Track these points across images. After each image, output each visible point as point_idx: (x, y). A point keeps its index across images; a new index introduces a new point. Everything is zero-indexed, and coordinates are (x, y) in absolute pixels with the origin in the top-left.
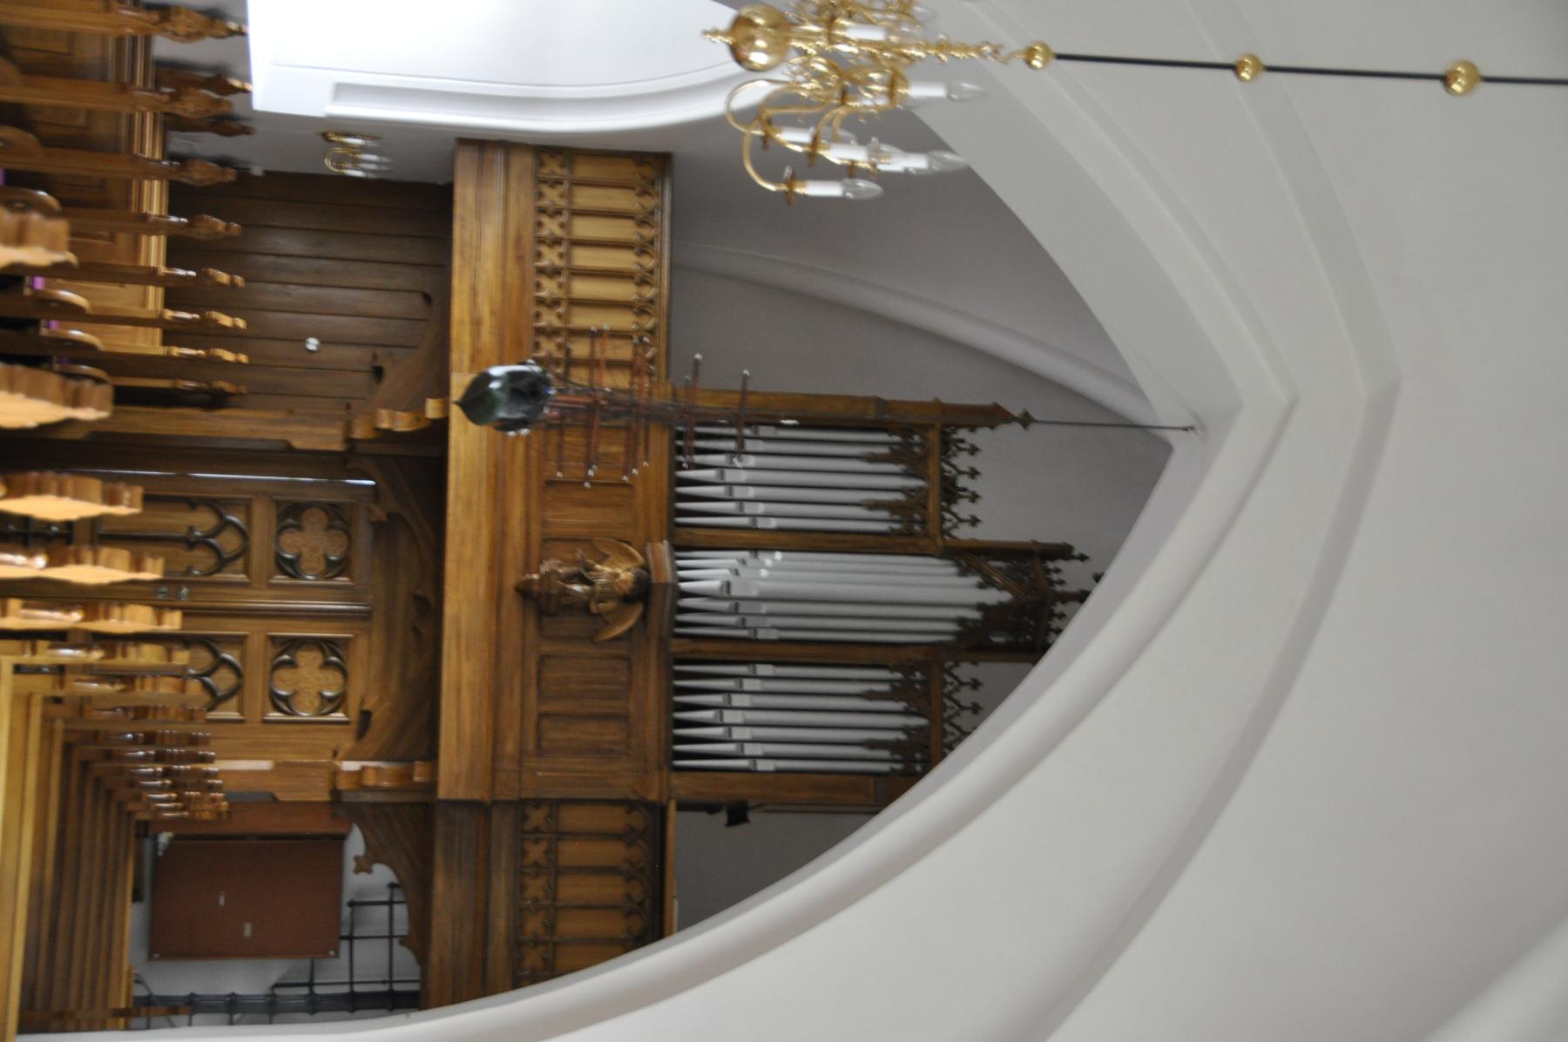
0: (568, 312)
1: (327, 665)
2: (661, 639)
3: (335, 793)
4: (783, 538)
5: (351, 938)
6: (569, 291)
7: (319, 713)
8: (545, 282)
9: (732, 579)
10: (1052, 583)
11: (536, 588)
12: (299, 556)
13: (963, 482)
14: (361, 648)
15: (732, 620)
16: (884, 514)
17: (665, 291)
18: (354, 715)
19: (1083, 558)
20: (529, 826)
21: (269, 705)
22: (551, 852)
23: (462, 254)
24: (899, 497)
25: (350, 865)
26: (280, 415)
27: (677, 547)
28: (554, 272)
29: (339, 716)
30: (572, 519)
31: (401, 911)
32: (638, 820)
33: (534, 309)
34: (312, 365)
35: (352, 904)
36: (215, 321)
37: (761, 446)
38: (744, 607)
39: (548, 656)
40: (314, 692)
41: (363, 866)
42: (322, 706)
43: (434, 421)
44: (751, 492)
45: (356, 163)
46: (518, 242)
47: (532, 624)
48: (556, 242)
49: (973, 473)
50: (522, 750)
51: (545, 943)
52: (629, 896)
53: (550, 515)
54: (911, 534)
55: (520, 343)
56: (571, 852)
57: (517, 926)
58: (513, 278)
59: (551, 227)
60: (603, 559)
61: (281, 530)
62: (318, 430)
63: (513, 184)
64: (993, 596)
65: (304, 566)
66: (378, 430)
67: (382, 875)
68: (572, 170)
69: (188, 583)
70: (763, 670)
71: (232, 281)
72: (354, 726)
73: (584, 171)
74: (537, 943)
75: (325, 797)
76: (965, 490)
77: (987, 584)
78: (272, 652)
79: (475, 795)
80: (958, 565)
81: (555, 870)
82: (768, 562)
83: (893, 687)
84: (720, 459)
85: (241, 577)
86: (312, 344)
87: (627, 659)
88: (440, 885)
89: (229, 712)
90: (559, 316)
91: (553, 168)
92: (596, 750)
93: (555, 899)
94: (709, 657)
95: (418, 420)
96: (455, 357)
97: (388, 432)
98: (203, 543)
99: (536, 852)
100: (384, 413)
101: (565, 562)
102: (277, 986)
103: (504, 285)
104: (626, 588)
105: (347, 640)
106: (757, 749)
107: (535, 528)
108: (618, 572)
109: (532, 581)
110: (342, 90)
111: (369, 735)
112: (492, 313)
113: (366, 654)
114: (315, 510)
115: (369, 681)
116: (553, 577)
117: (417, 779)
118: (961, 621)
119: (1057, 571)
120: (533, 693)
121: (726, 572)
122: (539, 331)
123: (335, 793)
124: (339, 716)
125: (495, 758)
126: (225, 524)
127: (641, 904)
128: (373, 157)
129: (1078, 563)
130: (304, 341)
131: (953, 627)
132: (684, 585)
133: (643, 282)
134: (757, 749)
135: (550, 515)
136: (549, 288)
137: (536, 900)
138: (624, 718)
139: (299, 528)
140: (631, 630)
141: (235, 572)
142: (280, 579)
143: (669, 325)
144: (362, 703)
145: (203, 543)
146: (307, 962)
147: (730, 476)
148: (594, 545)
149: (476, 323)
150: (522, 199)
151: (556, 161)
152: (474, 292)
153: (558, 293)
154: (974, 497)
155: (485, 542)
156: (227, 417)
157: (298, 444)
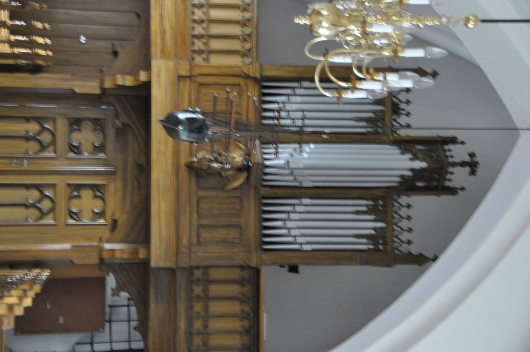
1: (96, 196)
5: (110, 322)
7: (93, 219)
8: (196, 11)
9: (290, 159)
10: (447, 157)
11: (196, 165)
13: (402, 106)
14: (112, 187)
16: (364, 240)
17: (255, 15)
18: (109, 221)
19: (462, 143)
20: (194, 278)
21: (68, 216)
22: (205, 290)
24: (371, 115)
25: (109, 292)
26: (69, 76)
28: (200, 52)
29: (102, 221)
31: (133, 309)
32: (246, 274)
33: (191, 25)
34: (84, 50)
35: (110, 307)
37: (303, 91)
38: (296, 172)
39: (202, 198)
41: (116, 292)
47: (194, 180)
49: (408, 102)
50: (190, 244)
51: (203, 334)
52: (243, 311)
54: (377, 133)
55: (184, 43)
56: (215, 290)
57: (190, 326)
61: (71, 131)
64: (419, 164)
65: (83, 148)
67: (124, 295)
69: (27, 158)
72: (109, 226)
74: (199, 333)
75: (96, 261)
76: (403, 110)
77: (415, 158)
78: (68, 190)
79: (169, 265)
80: (401, 148)
81: (206, 298)
82: (307, 150)
83: (369, 209)
85: (53, 155)
86: (83, 39)
87: (240, 198)
88: (153, 306)
89: (49, 220)
90: (204, 28)
92: (225, 242)
95: (136, 80)
98: (33, 138)
99: (198, 290)
102: (78, 344)
103: (177, 14)
104: (239, 164)
105: (104, 185)
109: (192, 162)
112: (171, 28)
113: (114, 190)
118: (402, 177)
119: (450, 150)
120: (195, 216)
122: (195, 36)
123: (102, 260)
124: (102, 221)
125: (178, 246)
126: (44, 129)
127: (249, 315)
129: (460, 146)
130: (78, 38)
131: (398, 179)
133: (245, 10)
137: (198, 313)
138: (238, 226)
139: (80, 130)
141: (49, 152)
142: (72, 155)
143: (257, 33)
144: (113, 215)
146: (90, 334)
149: (163, 33)
152: (162, 17)
153: (203, 17)
154: (408, 114)
157: (78, 90)
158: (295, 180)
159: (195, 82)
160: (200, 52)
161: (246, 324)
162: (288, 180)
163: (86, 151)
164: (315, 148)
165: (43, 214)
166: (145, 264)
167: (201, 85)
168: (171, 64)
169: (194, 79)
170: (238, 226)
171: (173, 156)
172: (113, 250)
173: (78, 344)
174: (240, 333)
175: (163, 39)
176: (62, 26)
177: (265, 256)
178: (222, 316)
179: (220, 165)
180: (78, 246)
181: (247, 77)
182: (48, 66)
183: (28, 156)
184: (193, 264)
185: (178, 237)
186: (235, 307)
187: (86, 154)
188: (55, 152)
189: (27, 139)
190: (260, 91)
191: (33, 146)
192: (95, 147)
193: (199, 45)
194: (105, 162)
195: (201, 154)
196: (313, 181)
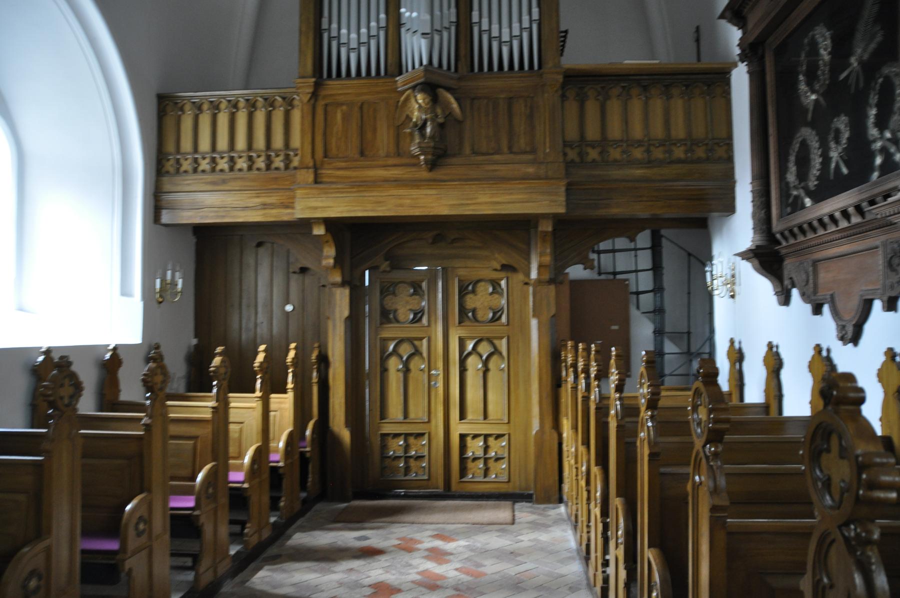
0: (256, 151)
1: (474, 291)
2: (459, 79)
3: (551, 281)
4: (391, 9)
6: (243, 152)
8: (238, 166)
12: (411, 310)
14: (462, 272)
15: (445, 34)
18: (502, 274)
20: (577, 160)
23: (223, 217)
27: (400, 73)
28: (287, 160)
30: (384, 138)
31: (603, 246)
34: (302, 307)
36: (261, 363)
39: (473, 149)
40: (490, 298)
42: (497, 293)
43: (327, 230)
44: (364, 30)
45: (174, 284)
46: (213, 183)
47: (454, 160)
48: (213, 160)
50: (533, 162)
53: (382, 153)
56: (592, 132)
58: (236, 185)
59: (205, 165)
60: (409, 118)
62: (338, 302)
63: (179, 188)
65: (416, 307)
66: (335, 266)
68: (170, 154)
69: (429, 371)
70: (475, 17)
71: (220, 354)
72: (509, 274)
73: (170, 147)
74: (648, 151)
75: (552, 287)
78: (467, 323)
81: (604, 143)
84: (343, 51)
85: (425, 342)
86: (289, 308)
87: (473, 99)
89: (503, 345)
91: (170, 166)
92: (531, 117)
93: (622, 141)
94: (469, 49)
96: (285, 218)
97: (336, 259)
98: (406, 364)
99: (593, 154)
100: (324, 262)
101: (412, 139)
105: (460, 281)
106: (526, 18)
107: (391, 161)
108: (418, 106)
109: (426, 161)
110: (125, 292)
111: (516, 266)
113: (466, 270)
114: (385, 303)
115: (483, 266)
116: (423, 145)
117: (550, 229)
120: (497, 157)
121: (415, 38)
122: (268, 167)
123: (551, 281)
124: (503, 283)
126: (395, 352)
127: (623, 87)
128: (169, 273)
130: (288, 313)
132: (425, 62)
133: (235, 106)
134: (526, 18)
135: (382, 153)
136: (242, 164)
137: (624, 152)
138: (510, 101)
139: (396, 311)
140: (457, 99)
141: (422, 345)
142: (425, 320)
144: (496, 270)
145: (486, 363)
147: (354, 45)
148: (400, 126)
149: (265, 206)
150: (189, 182)
151: (163, 165)
155: (401, 192)
156: (333, 350)
157: (346, 313)
158: (448, 29)
159: (322, 163)
160: (287, 160)
161: (635, 91)
162: (448, 38)
163: (420, 303)
164: (405, 7)
165: (496, 351)
166: (559, 221)
167: (326, 156)
168: (299, 193)
169: (318, 163)
170: (510, 101)
171: (418, 187)
172: (540, 267)
173: (638, 308)
174: (647, 98)
175: (272, 206)
176: (275, 330)
177: (549, 65)
178: (626, 122)
179: (429, 123)
180: (534, 311)
181: (315, 95)
182: (319, 347)
183: (426, 369)
184: (561, 159)
185: (525, 178)
186: (614, 107)
187: (423, 304)
188: (421, 339)
189: (407, 371)
190: (334, 80)
191: (418, 365)
192: (415, 293)
193: (278, 162)
194: (431, 277)
195: (414, 149)
196: (449, 7)
